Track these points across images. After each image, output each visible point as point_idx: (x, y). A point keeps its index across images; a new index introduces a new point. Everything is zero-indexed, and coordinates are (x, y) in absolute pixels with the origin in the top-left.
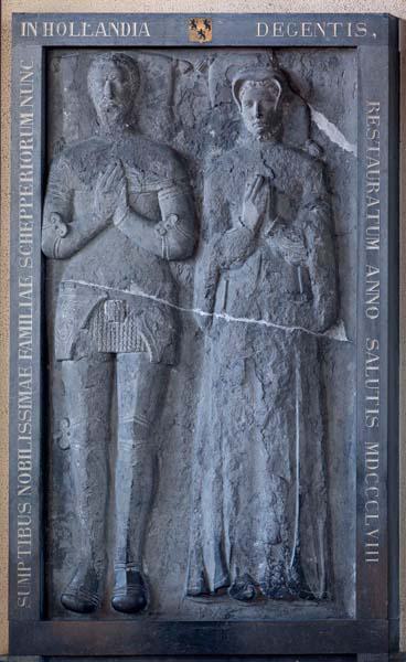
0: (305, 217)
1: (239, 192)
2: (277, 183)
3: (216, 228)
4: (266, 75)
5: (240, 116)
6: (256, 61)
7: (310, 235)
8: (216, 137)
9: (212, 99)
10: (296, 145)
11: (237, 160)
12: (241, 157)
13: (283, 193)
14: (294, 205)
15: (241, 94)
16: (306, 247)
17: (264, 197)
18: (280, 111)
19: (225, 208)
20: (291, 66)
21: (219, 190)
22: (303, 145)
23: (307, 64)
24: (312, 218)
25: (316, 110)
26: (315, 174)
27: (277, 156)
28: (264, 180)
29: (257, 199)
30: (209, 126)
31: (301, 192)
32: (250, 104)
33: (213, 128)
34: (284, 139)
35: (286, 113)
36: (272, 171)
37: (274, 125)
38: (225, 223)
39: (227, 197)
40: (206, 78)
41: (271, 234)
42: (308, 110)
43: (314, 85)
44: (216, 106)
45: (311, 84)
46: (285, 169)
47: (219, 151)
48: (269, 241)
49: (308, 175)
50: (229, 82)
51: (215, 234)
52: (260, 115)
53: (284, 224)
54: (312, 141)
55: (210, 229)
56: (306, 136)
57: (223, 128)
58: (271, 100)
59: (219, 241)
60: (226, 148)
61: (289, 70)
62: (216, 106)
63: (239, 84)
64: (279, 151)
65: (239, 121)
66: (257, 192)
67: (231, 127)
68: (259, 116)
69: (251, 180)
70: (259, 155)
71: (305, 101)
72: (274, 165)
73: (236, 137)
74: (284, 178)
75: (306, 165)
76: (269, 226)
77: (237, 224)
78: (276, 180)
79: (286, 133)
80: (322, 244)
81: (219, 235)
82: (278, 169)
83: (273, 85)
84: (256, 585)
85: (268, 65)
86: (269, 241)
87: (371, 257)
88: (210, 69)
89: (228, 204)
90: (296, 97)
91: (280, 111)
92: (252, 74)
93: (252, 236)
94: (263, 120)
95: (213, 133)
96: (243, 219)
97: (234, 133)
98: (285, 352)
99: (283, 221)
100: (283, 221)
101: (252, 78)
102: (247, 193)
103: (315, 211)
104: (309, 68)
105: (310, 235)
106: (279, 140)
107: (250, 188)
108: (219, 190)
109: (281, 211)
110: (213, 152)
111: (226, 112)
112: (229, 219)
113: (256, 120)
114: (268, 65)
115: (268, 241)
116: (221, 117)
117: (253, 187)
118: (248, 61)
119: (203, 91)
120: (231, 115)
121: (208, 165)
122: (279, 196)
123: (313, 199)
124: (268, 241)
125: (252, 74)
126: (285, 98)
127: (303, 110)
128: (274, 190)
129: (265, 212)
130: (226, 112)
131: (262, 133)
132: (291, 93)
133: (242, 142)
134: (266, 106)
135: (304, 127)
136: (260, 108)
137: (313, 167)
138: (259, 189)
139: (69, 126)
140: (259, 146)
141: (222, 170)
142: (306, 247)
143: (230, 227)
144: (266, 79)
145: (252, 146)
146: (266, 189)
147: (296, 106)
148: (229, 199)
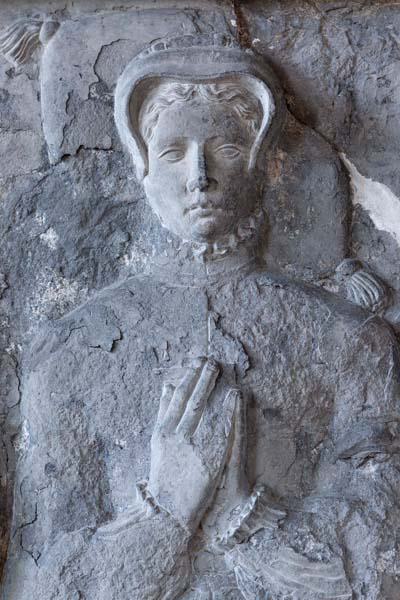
0: (340, 489)
1: (141, 410)
2: (258, 383)
3: (66, 518)
4: (225, 67)
5: (138, 187)
6: (188, 28)
7: (362, 541)
8: (61, 250)
9: (52, 138)
10: (308, 276)
11: (133, 315)
13: (275, 413)
14: (307, 450)
15: (146, 119)
16: (350, 579)
18: (260, 173)
19: (94, 457)
21: (76, 403)
22: (326, 276)
23: (339, 42)
24: (364, 491)
25: (366, 175)
26: (371, 358)
27: (256, 305)
29: (202, 429)
30: (40, 219)
31: (326, 414)
32: (178, 148)
33: (52, 224)
34: (269, 258)
35: (275, 180)
36: (245, 350)
37: (245, 212)
38: (92, 502)
39: (98, 425)
40: (33, 77)
41: (241, 537)
42: (344, 175)
43: (360, 96)
44: (65, 157)
45: (352, 96)
46: (283, 343)
47: (69, 290)
48: (235, 562)
49: (351, 362)
50: (105, 88)
51: (63, 537)
52: (208, 183)
53: (283, 507)
54: (358, 265)
55: (45, 524)
56: (337, 248)
57: (83, 224)
58: (240, 138)
59: (75, 558)
60: (93, 282)
61: (281, 58)
62: (65, 157)
63: (140, 94)
64: (260, 290)
65: (133, 204)
66: (199, 410)
67: (106, 222)
69: (179, 376)
70: (201, 301)
71: (336, 149)
72: (248, 329)
73: (125, 249)
74: (279, 369)
75: (344, 332)
76: (236, 512)
77: (130, 505)
78: (255, 375)
79: (278, 236)
81: (77, 538)
82: (261, 341)
83: (245, 96)
85: (224, 40)
86: (235, 562)
87: (100, 209)
88: (48, 51)
89: (100, 445)
90: (305, 131)
91: (260, 173)
92: (180, 63)
93: (183, 543)
95: (50, 237)
96: (152, 489)
97: (119, 238)
99: (272, 497)
100: (272, 497)
101: (183, 76)
102: (163, 414)
103: (371, 469)
104: (344, 52)
105: (362, 541)
106: (257, 255)
107: (177, 396)
108: (76, 403)
109: (268, 471)
110: (50, 292)
111: (93, 176)
112: (105, 491)
113: (197, 196)
114: (224, 40)
115: (228, 557)
116: (79, 191)
117: (187, 396)
118: (163, 30)
119: (24, 114)
121: (36, 332)
122: (265, 425)
123: (366, 433)
124: (228, 557)
125: (180, 63)
126: (281, 137)
127: (330, 171)
128: (250, 402)
129: (225, 469)
130: (93, 176)
131: (210, 236)
132: (291, 122)
133: (142, 262)
134: (224, 157)
135: (332, 221)
136: (207, 162)
137: (365, 337)
138: (207, 402)
139: (367, 350)
140: (199, 273)
141: (85, 343)
142: (350, 579)
143: (107, 516)
144: (226, 77)
146: (229, 401)
147: (307, 160)
148: (106, 433)
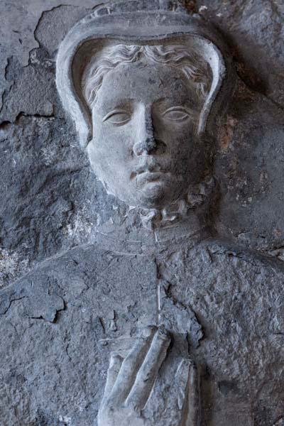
1: (85, 382)
2: (213, 353)
5: (81, 154)
10: (263, 245)
11: (78, 285)
12: (90, 279)
13: (230, 385)
15: (90, 82)
17: (178, 395)
18: (209, 139)
20: (236, 14)
27: (208, 273)
28: (173, 346)
29: (153, 402)
32: (123, 111)
34: (220, 227)
35: (226, 147)
36: (198, 318)
46: (238, 312)
57: (23, 193)
58: (189, 101)
60: (33, 253)
61: (231, 26)
64: (212, 258)
66: (149, 381)
68: (155, 147)
69: (128, 346)
70: (150, 269)
72: (200, 298)
73: (68, 219)
74: (235, 339)
78: (209, 346)
79: (231, 204)
80: (101, 150)
82: (214, 311)
84: (155, 65)
91: (209, 139)
92: (125, 26)
94: (166, 159)
97: (62, 207)
98: (184, 395)
102: (111, 386)
106: (207, 222)
107: (126, 367)
111: (34, 143)
113: (144, 159)
117: (137, 367)
120: (49, 154)
122: (221, 398)
125: (125, 26)
128: (204, 374)
130: (34, 143)
131: (159, 201)
132: (243, 89)
133: (85, 232)
134: (173, 120)
136: (154, 124)
140: (148, 241)
145: (125, 244)
146: (182, 371)
147: (259, 126)
